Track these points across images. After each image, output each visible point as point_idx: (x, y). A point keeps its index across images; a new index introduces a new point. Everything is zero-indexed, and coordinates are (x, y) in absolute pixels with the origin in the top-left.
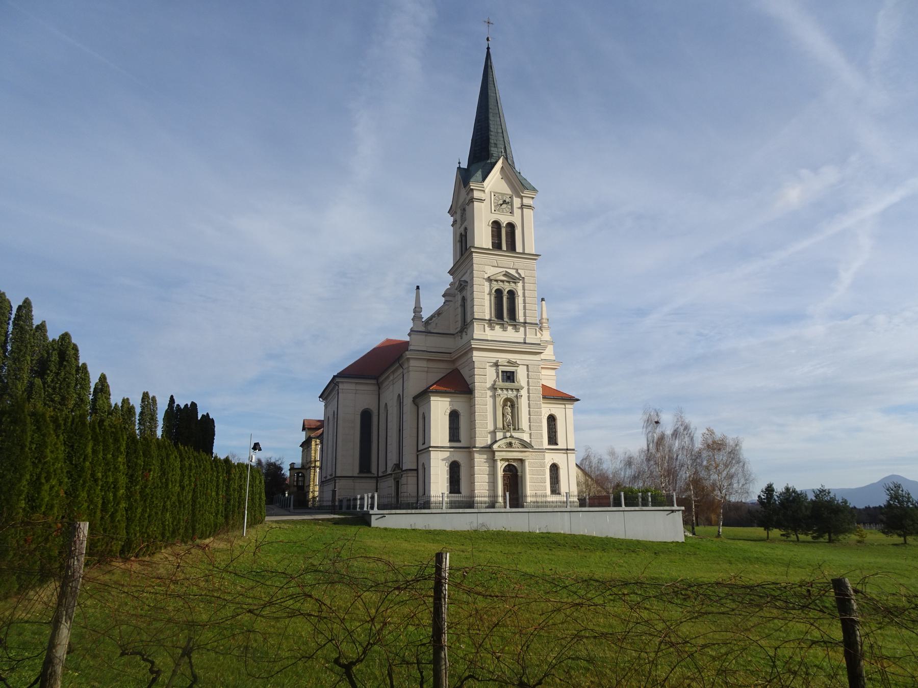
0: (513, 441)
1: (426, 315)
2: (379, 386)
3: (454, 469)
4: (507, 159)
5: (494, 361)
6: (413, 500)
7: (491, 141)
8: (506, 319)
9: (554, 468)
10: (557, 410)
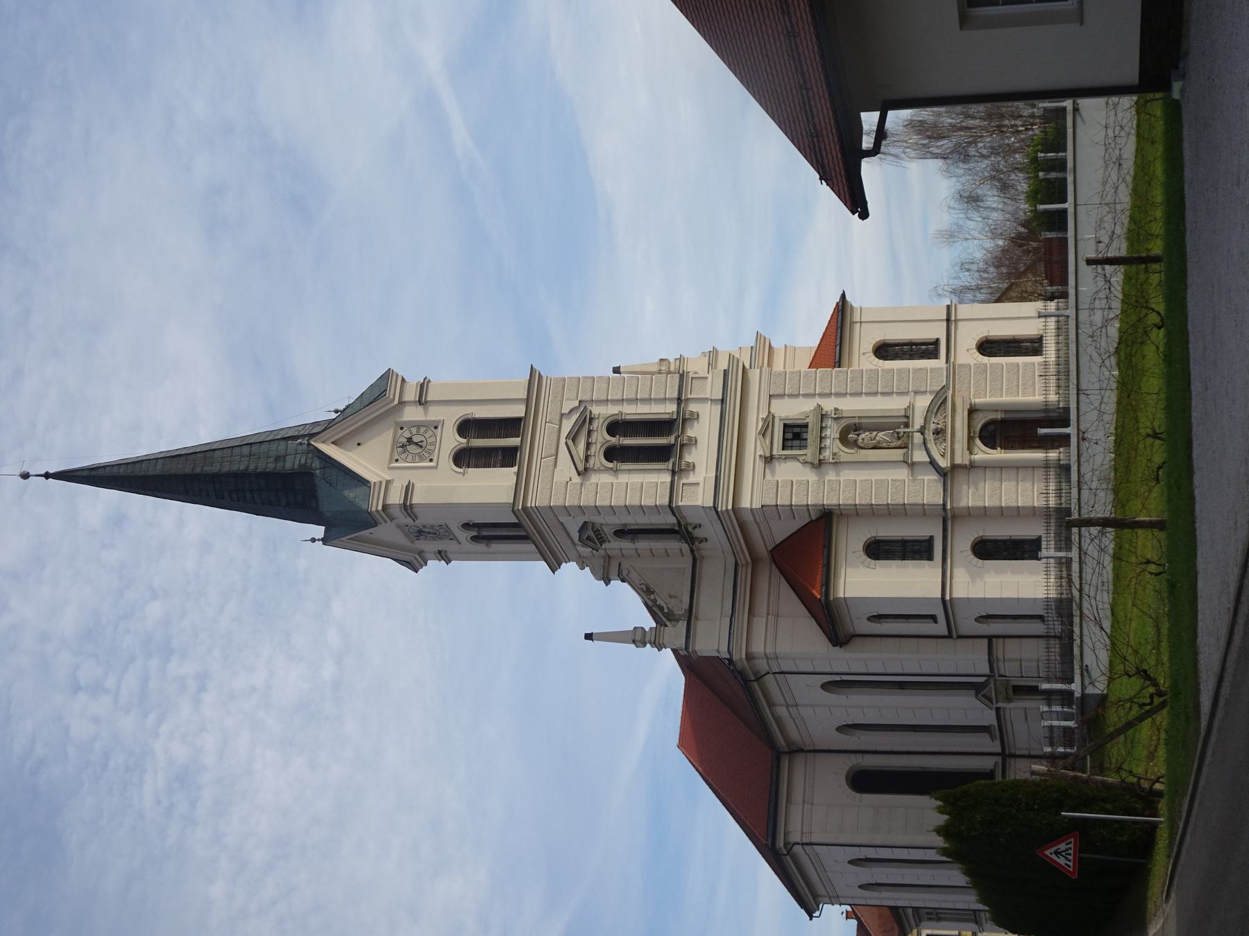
0: (933, 426)
1: (648, 623)
2: (796, 750)
3: (986, 550)
4: (312, 436)
5: (760, 464)
6: (1056, 646)
7: (271, 467)
8: (670, 440)
9: (988, 347)
10: (864, 340)
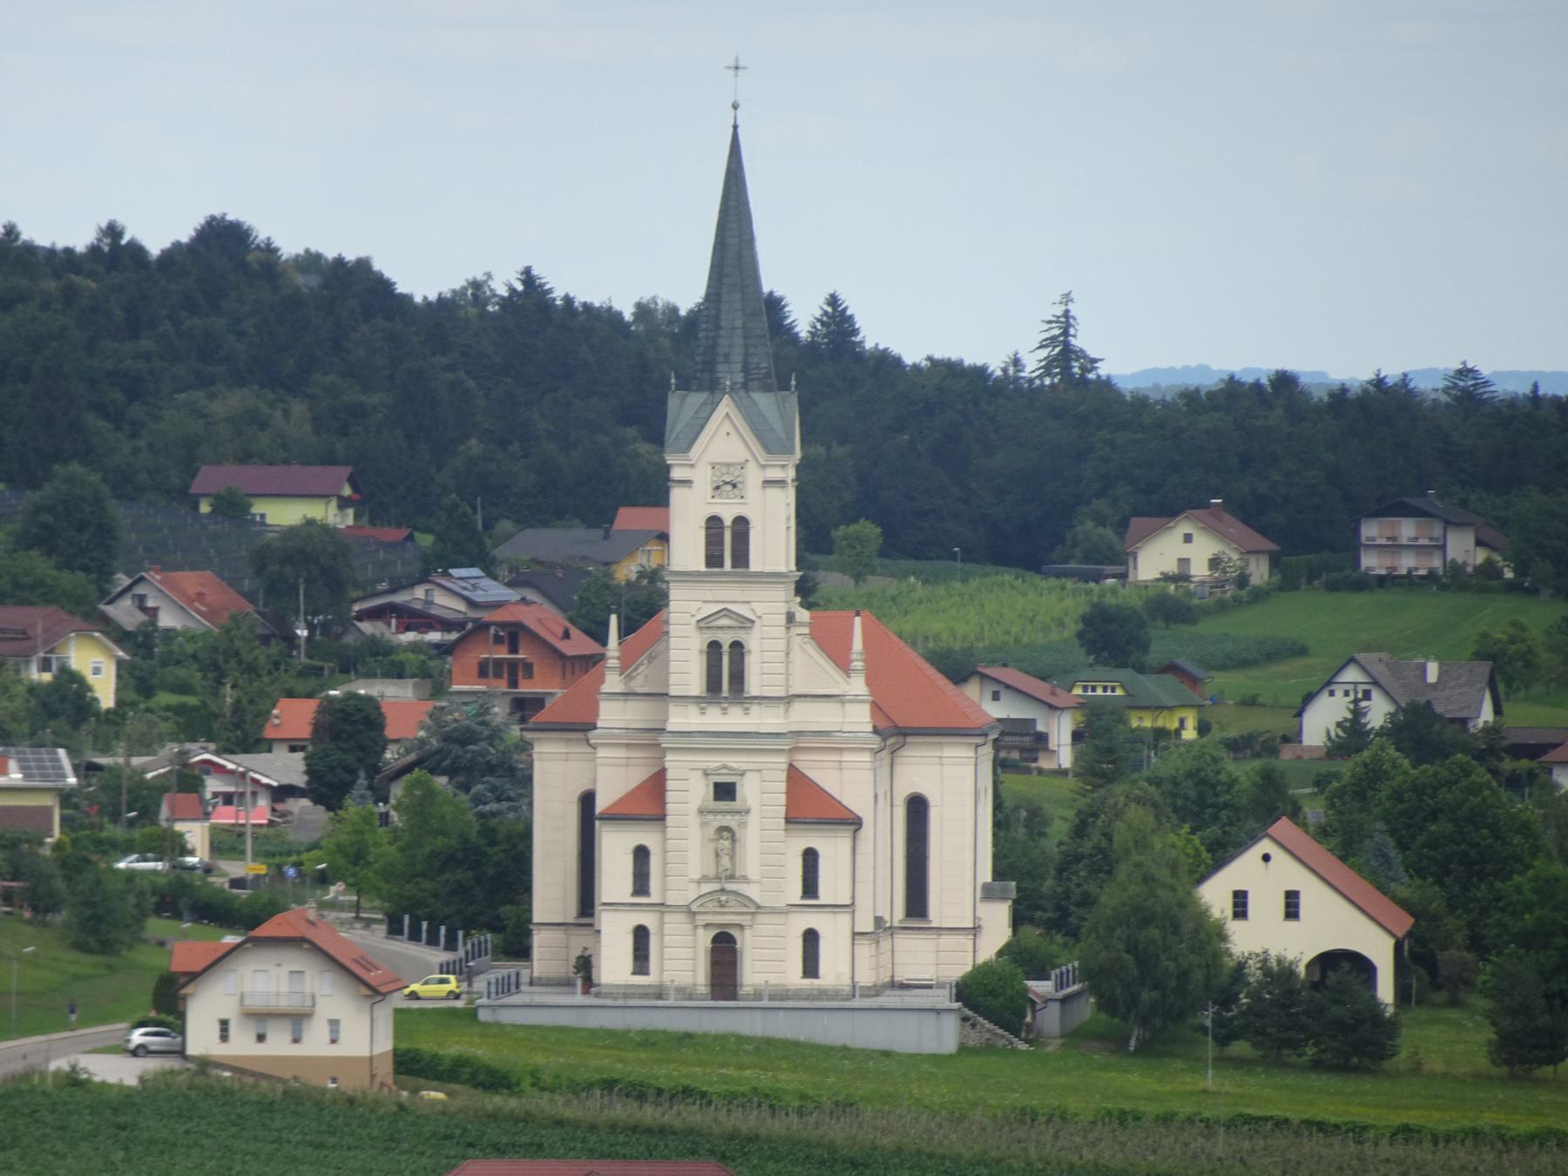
7: (720, 350)
